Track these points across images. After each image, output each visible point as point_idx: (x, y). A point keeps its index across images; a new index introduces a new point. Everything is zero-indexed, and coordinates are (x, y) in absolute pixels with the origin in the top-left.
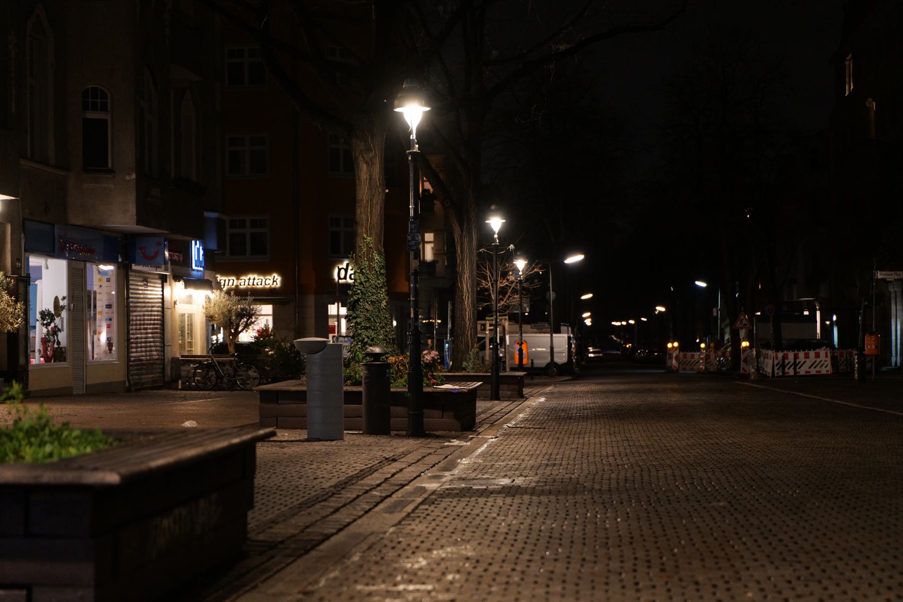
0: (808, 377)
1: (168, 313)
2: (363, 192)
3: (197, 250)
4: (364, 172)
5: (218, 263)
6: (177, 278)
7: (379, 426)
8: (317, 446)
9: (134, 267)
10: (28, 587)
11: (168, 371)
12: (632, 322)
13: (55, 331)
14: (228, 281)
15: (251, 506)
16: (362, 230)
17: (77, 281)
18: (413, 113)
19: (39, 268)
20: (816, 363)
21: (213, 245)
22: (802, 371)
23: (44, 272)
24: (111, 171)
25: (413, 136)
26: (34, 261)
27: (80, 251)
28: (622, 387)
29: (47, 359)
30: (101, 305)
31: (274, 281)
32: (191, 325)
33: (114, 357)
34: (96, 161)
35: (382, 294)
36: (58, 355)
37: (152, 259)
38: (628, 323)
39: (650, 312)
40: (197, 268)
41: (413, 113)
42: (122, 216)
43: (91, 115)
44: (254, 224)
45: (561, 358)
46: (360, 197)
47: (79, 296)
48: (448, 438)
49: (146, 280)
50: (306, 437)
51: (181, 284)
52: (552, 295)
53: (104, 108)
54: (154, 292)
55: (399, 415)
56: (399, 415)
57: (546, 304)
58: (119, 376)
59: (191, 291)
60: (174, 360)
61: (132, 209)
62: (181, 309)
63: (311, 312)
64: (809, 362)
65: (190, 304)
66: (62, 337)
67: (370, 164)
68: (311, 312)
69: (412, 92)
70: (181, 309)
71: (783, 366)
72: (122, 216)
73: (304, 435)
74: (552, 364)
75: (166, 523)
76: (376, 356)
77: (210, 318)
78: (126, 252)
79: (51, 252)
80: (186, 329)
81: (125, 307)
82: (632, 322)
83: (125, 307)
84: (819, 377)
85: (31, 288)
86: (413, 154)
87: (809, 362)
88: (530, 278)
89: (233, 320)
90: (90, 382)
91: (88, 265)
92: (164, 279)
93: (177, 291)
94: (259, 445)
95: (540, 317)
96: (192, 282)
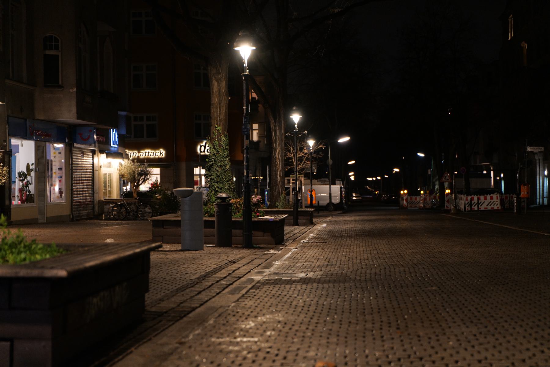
0: (486, 211)
1: (96, 173)
2: (215, 99)
3: (113, 135)
4: (215, 86)
5: (126, 142)
6: (101, 152)
7: (225, 242)
8: (187, 254)
10: (11, 340)
11: (96, 208)
13: (28, 184)
14: (133, 154)
15: (147, 290)
16: (214, 122)
18: (245, 50)
20: (491, 203)
21: (123, 132)
22: (482, 208)
24: (61, 87)
25: (246, 65)
26: (14, 142)
27: (42, 135)
29: (23, 202)
30: (55, 168)
32: (110, 181)
33: (63, 200)
34: (52, 81)
35: (227, 161)
36: (29, 199)
37: (86, 141)
40: (114, 146)
41: (245, 50)
42: (68, 114)
43: (48, 52)
45: (336, 200)
47: (42, 163)
48: (267, 249)
49: (83, 153)
50: (180, 248)
51: (104, 156)
52: (330, 162)
53: (57, 48)
54: (87, 160)
57: (326, 167)
58: (67, 212)
59: (110, 160)
60: (100, 202)
61: (74, 109)
62: (104, 170)
63: (183, 173)
64: (487, 202)
65: (110, 167)
66: (32, 188)
67: (219, 82)
68: (183, 173)
69: (245, 38)
70: (104, 170)
71: (471, 204)
72: (68, 114)
73: (179, 247)
74: (331, 203)
75: (95, 300)
76: (223, 199)
77: (122, 176)
78: (71, 136)
79: (25, 136)
80: (107, 183)
81: (70, 170)
83: (70, 170)
84: (492, 211)
85: (12, 158)
86: (246, 75)
87: (487, 202)
88: (317, 151)
89: (135, 178)
90: (49, 215)
91: (47, 144)
92: (93, 152)
93: (101, 160)
95: (323, 175)
96: (110, 154)
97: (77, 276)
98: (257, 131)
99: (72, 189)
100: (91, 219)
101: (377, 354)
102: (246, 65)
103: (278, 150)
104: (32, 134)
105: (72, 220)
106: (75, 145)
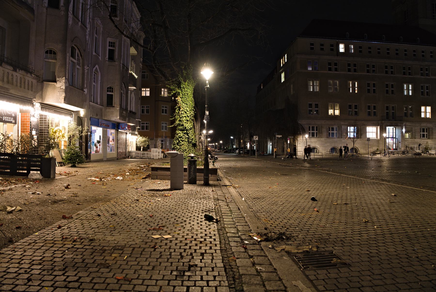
1: (127, 141)
9: (119, 130)
11: (127, 154)
12: (217, 144)
17: (105, 133)
19: (95, 131)
23: (97, 131)
24: (114, 107)
25: (207, 82)
26: (94, 128)
28: (224, 159)
31: (410, 94)
38: (215, 144)
39: (218, 143)
42: (116, 118)
44: (146, 124)
46: (46, 186)
47: (105, 138)
50: (169, 187)
53: (112, 92)
54: (123, 136)
55: (200, 176)
56: (200, 176)
58: (115, 156)
72: (116, 118)
76: (192, 157)
78: (117, 126)
79: (98, 125)
81: (117, 140)
82: (217, 144)
83: (117, 140)
91: (108, 129)
94: (187, 270)
97: (139, 12)
98: (333, 114)
99: (96, 201)
100: (125, 158)
101: (270, 246)
102: (207, 82)
103: (86, 124)
104: (101, 125)
105: (118, 159)
106: (119, 130)
